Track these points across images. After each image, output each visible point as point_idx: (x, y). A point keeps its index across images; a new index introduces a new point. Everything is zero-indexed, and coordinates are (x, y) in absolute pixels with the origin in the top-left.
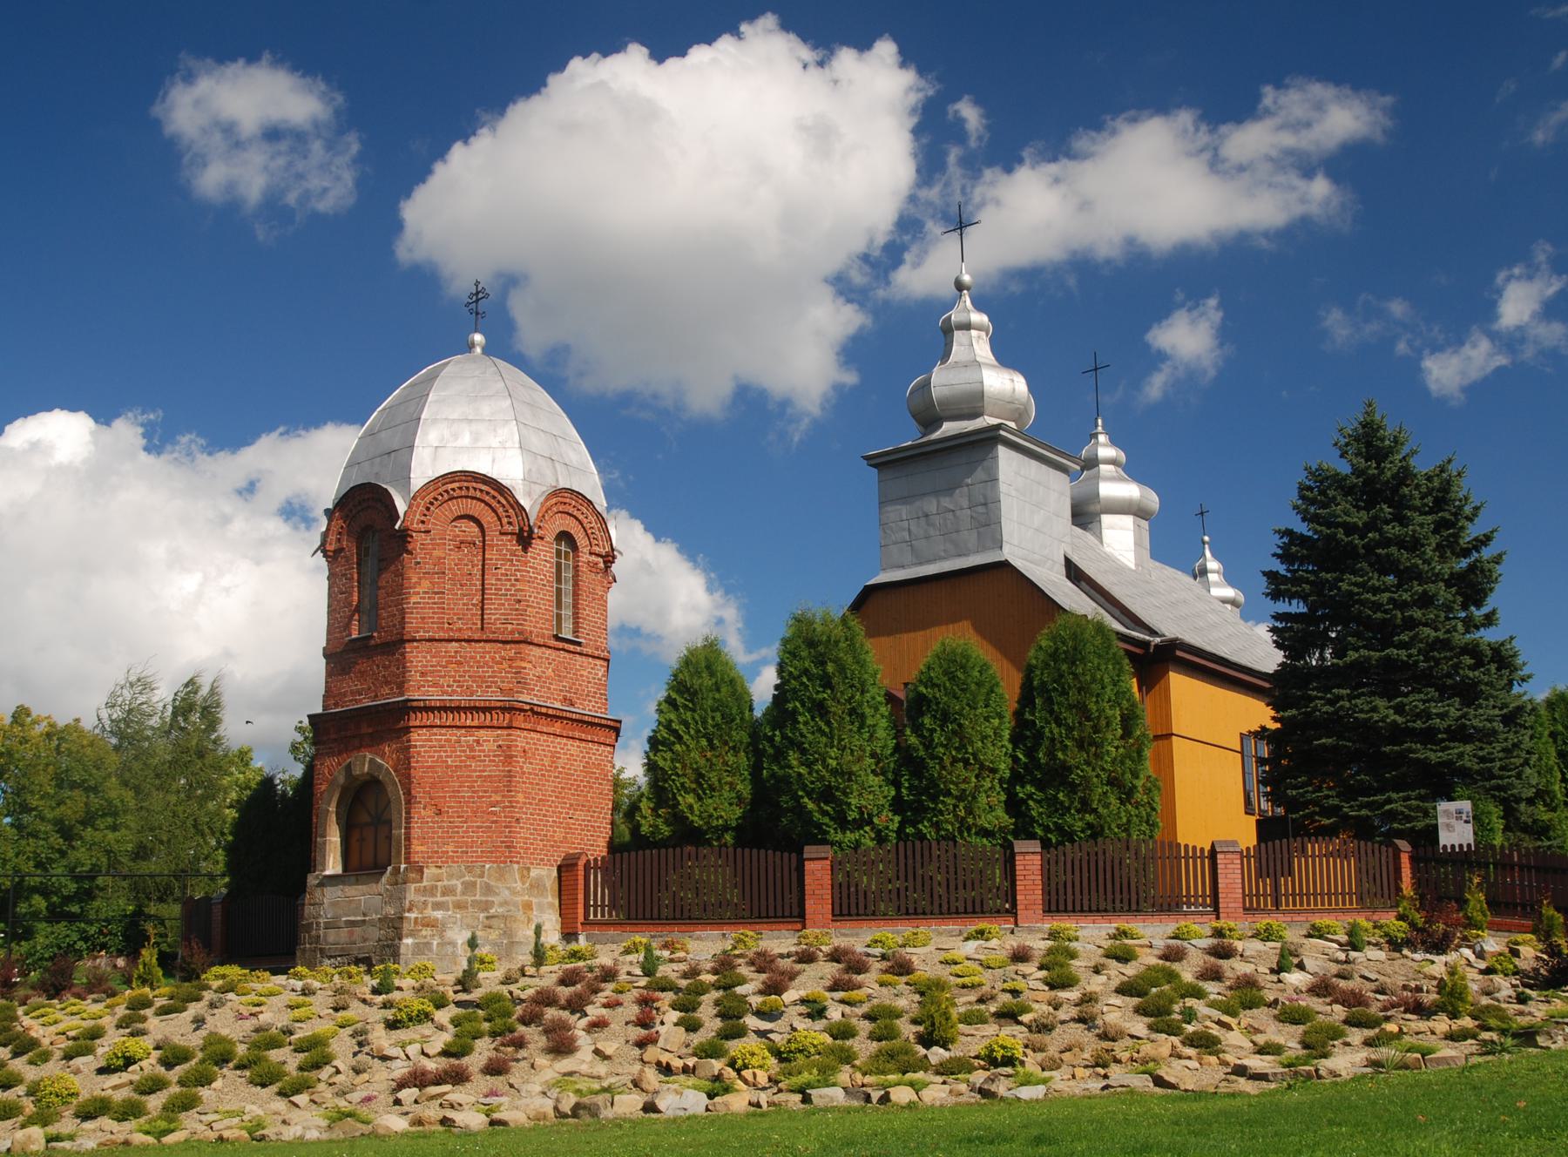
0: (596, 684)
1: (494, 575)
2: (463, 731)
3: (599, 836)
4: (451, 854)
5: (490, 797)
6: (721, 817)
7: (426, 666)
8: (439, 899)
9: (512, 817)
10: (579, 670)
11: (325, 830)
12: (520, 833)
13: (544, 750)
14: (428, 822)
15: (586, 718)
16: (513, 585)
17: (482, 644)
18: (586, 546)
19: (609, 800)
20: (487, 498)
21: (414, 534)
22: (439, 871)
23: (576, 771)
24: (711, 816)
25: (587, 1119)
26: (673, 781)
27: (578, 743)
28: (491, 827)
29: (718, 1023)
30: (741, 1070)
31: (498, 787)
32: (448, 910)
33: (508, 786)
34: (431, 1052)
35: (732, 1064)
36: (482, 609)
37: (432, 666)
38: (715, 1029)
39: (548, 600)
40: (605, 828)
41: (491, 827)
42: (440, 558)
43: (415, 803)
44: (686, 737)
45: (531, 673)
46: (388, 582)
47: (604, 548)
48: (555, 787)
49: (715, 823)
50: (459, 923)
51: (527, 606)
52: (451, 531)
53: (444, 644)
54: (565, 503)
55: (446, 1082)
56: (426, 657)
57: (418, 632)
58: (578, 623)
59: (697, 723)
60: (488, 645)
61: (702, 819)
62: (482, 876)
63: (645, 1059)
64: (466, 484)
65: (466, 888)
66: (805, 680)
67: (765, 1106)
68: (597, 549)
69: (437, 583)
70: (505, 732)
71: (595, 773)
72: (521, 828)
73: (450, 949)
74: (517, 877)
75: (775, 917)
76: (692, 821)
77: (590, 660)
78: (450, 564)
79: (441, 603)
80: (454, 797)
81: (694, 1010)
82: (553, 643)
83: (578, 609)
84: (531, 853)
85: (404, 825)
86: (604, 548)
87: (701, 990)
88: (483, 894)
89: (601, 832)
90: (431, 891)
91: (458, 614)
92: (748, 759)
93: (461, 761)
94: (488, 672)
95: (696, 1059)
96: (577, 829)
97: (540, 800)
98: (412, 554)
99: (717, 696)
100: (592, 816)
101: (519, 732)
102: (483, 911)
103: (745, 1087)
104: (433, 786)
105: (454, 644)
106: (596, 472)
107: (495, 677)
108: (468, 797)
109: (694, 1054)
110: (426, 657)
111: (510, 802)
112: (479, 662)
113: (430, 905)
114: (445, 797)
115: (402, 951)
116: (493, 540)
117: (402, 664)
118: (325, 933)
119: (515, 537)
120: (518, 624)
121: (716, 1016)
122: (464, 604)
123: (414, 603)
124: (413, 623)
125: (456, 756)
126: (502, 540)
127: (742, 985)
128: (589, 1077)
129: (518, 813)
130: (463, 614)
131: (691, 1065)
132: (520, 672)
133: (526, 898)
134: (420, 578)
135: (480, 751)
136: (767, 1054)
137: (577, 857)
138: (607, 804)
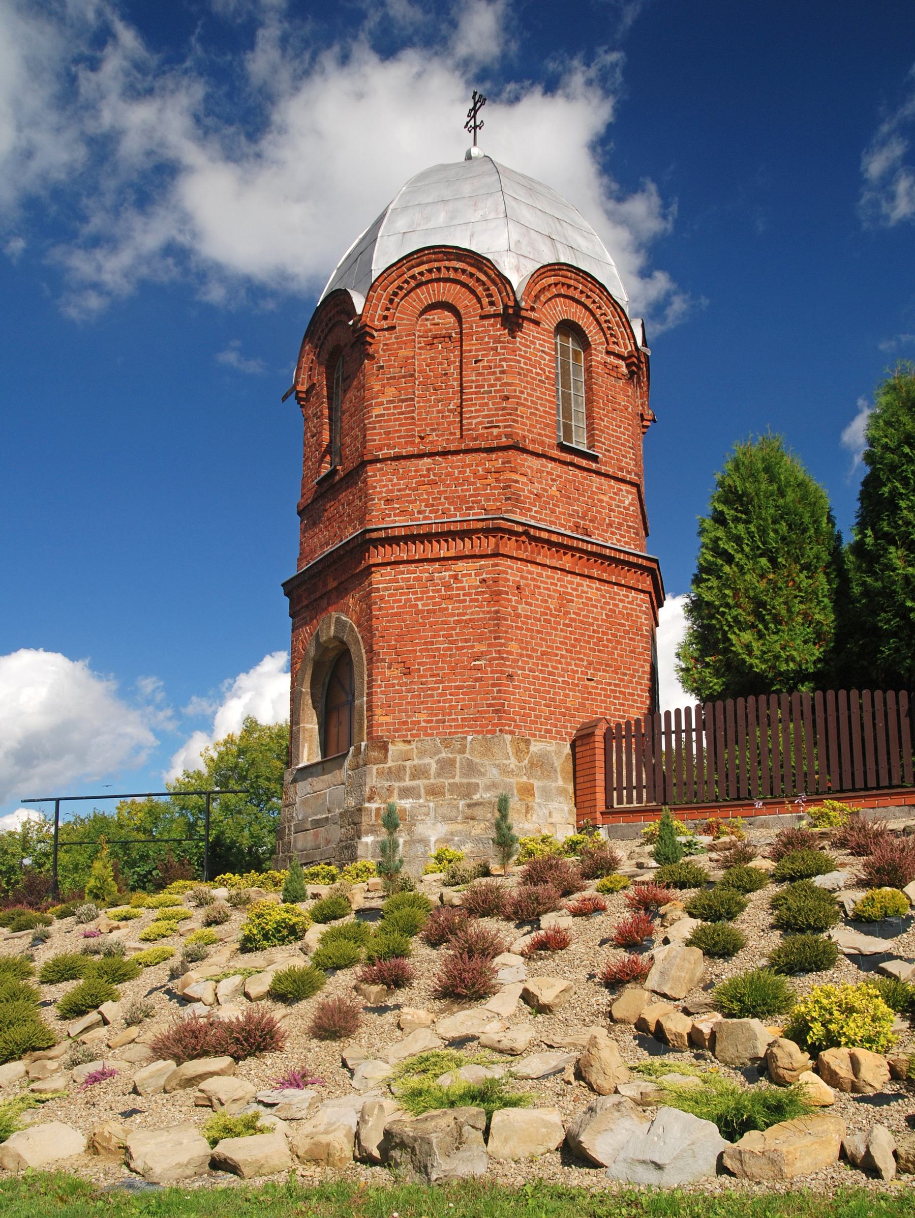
0: (621, 513)
1: (473, 369)
2: (437, 565)
3: (632, 706)
4: (423, 724)
5: (473, 647)
6: (793, 659)
7: (392, 491)
8: (408, 783)
9: (502, 672)
10: (596, 493)
11: (298, 718)
12: (514, 694)
13: (548, 589)
14: (393, 685)
15: (632, 559)
16: (497, 379)
17: (461, 456)
18: (601, 344)
19: (645, 660)
20: (463, 278)
21: (375, 334)
22: (408, 747)
23: (595, 619)
24: (777, 657)
25: (407, 1171)
26: (723, 614)
27: (597, 584)
28: (474, 687)
29: (776, 939)
30: (821, 1048)
31: (482, 633)
32: (419, 797)
33: (495, 631)
34: (254, 991)
35: (798, 1033)
36: (461, 414)
37: (399, 490)
38: (768, 950)
39: (547, 400)
40: (640, 696)
41: (474, 687)
42: (408, 358)
43: (378, 661)
44: (738, 556)
45: (526, 490)
46: (351, 402)
47: (626, 348)
48: (565, 637)
49: (784, 667)
50: (432, 814)
51: (518, 404)
52: (421, 325)
53: (415, 461)
54: (569, 286)
55: (218, 1052)
56: (391, 480)
57: (381, 450)
58: (593, 435)
59: (752, 537)
60: (468, 458)
61: (765, 661)
62: (462, 751)
63: (617, 1014)
64: (436, 265)
65: (442, 768)
66: (907, 450)
67: (888, 1166)
68: (616, 349)
69: (405, 388)
70: (490, 562)
71: (624, 625)
72: (515, 687)
73: (420, 849)
74: (510, 750)
75: (878, 788)
76: (751, 666)
77: (612, 482)
78: (420, 365)
79: (409, 412)
80: (427, 650)
81: (731, 916)
82: (556, 453)
83: (593, 418)
84: (532, 722)
85: (366, 691)
86: (626, 348)
87: (751, 883)
88: (464, 775)
89: (634, 701)
90: (397, 773)
91: (432, 424)
92: (829, 582)
93: (434, 604)
94: (469, 490)
95: (718, 1017)
96: (600, 695)
97: (543, 653)
98: (374, 358)
99: (781, 502)
100: (622, 680)
101: (509, 562)
102: (463, 798)
103: (828, 1093)
104: (400, 637)
105: (426, 460)
106: (613, 264)
107: (478, 495)
108: (445, 649)
109: (717, 1007)
110: (391, 480)
111: (499, 652)
112: (457, 479)
113: (396, 792)
114: (416, 651)
115: (360, 851)
116: (472, 328)
117: (365, 497)
118: (295, 838)
119: (499, 320)
120: (506, 427)
121: (773, 927)
122: (439, 412)
123: (377, 416)
124: (375, 438)
125: (428, 598)
126: (483, 326)
127: (824, 873)
128: (494, 1049)
129: (510, 666)
130: (438, 424)
131: (706, 1031)
132: (510, 487)
133: (525, 779)
134: (383, 386)
135: (458, 589)
136: (884, 1008)
137: (594, 724)
138: (643, 666)
